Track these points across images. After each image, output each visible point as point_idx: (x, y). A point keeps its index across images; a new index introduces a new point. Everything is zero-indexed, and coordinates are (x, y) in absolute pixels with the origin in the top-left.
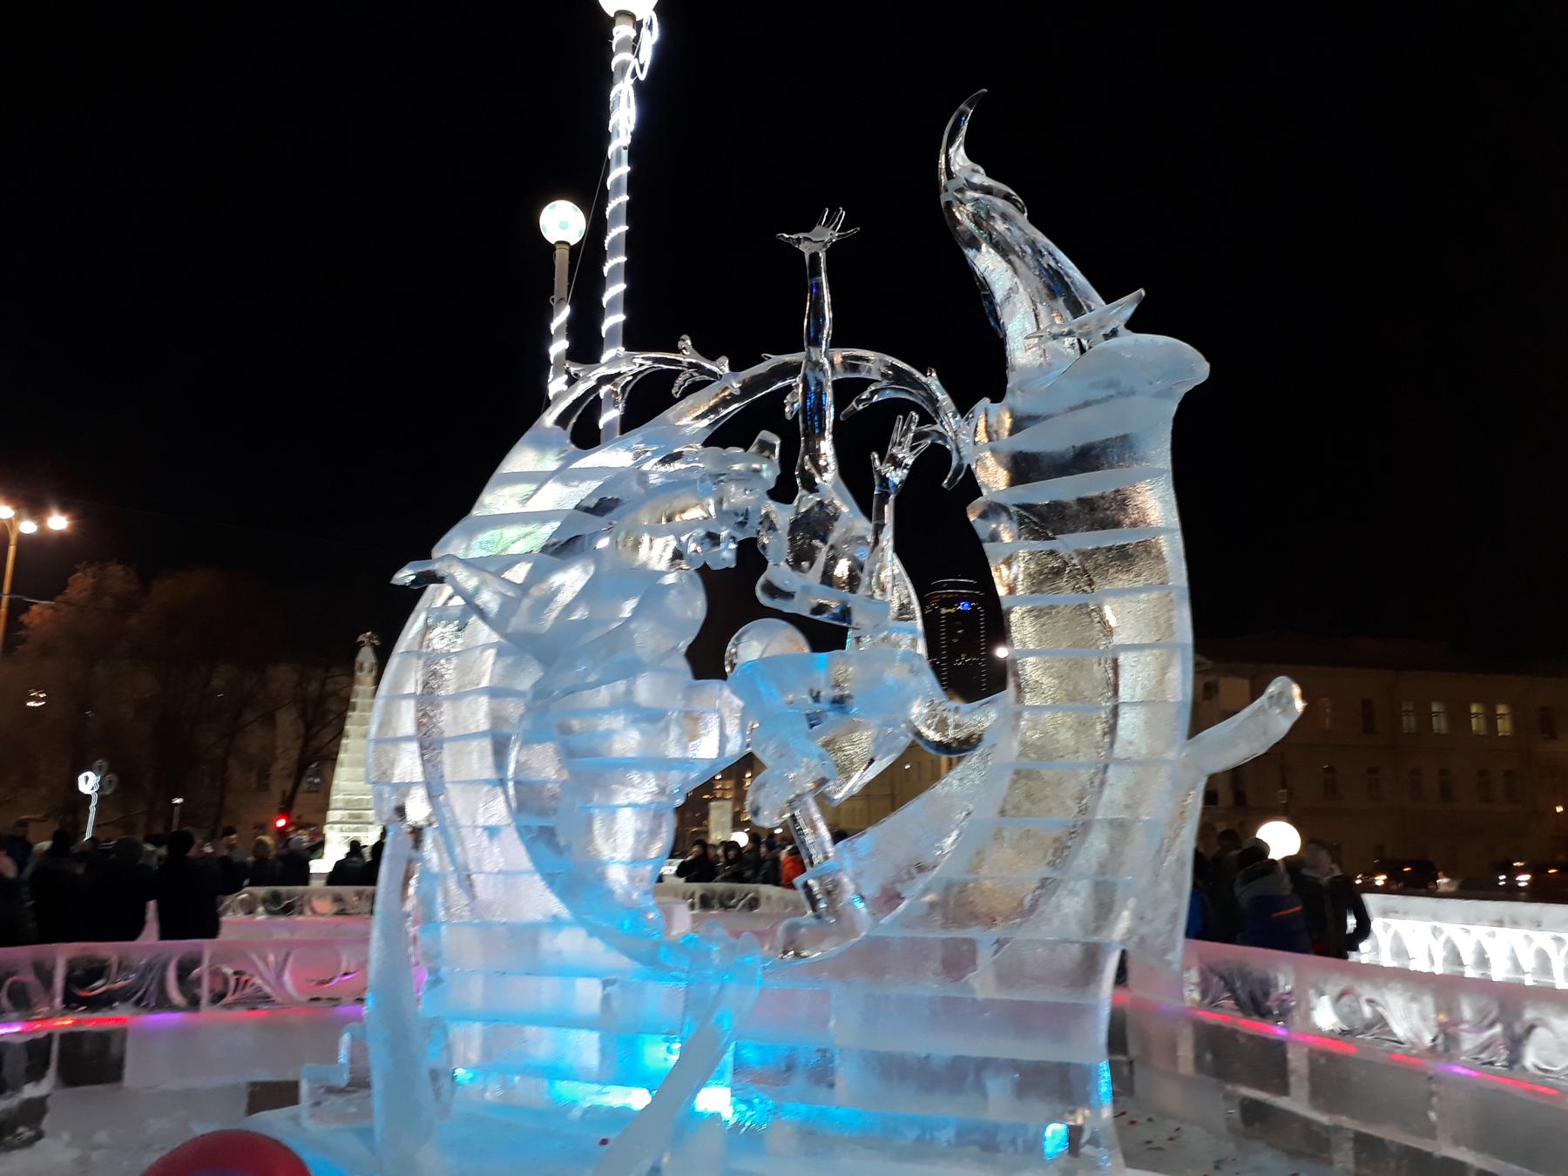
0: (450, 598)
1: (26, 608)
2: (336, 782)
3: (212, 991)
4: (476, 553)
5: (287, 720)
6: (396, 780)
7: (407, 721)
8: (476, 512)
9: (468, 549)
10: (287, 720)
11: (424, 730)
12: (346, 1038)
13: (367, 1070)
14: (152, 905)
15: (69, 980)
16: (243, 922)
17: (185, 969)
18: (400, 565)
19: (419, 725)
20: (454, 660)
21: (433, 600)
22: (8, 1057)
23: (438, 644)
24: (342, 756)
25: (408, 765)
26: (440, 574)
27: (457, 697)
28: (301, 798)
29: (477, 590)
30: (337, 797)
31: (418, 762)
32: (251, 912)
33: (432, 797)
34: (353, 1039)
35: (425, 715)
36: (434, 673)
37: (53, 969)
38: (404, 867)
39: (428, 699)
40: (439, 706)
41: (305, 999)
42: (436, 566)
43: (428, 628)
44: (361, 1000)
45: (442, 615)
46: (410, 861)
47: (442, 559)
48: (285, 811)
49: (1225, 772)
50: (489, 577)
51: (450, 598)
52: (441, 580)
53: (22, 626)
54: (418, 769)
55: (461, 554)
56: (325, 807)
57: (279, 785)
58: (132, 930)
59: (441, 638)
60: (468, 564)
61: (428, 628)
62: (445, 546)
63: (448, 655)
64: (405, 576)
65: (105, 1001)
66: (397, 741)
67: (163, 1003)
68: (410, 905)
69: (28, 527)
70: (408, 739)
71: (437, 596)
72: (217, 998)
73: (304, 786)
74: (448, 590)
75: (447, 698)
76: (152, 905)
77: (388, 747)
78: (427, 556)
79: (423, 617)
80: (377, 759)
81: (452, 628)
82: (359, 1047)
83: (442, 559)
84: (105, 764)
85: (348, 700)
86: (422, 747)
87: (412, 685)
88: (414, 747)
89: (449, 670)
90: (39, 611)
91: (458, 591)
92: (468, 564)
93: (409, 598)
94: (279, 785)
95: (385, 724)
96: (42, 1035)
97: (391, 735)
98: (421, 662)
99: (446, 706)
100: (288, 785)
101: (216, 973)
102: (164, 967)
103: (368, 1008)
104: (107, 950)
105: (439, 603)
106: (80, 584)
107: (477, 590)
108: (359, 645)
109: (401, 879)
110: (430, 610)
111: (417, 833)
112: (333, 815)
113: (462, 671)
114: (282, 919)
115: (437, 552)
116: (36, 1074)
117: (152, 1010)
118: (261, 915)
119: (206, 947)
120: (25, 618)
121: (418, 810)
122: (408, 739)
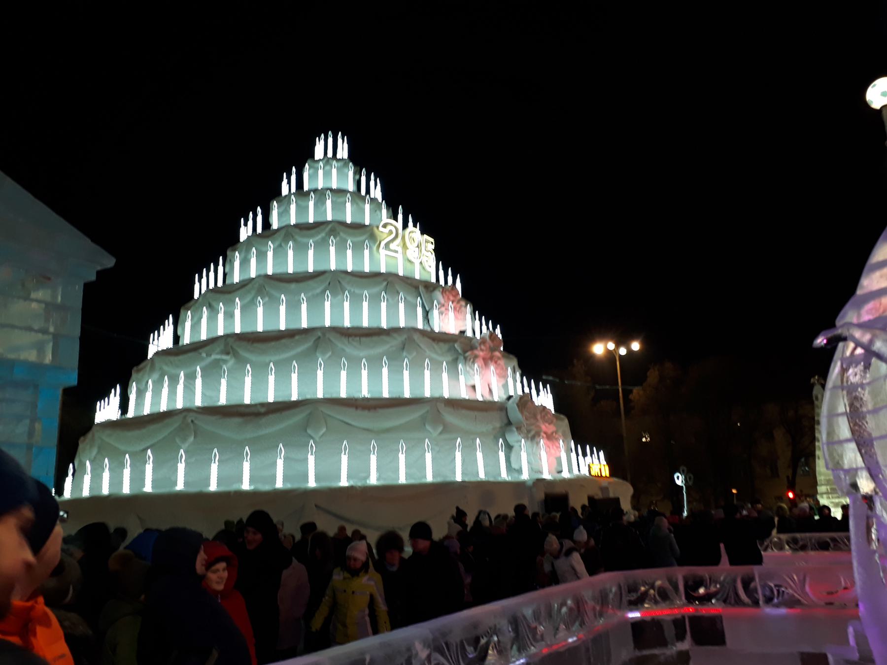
0: (855, 349)
1: (631, 391)
2: (817, 469)
3: (764, 596)
4: (866, 317)
5: (779, 435)
6: (846, 467)
7: (844, 430)
8: (859, 292)
9: (859, 316)
10: (779, 435)
11: (857, 434)
12: (851, 630)
13: (870, 651)
14: (722, 546)
15: (686, 586)
16: (778, 557)
17: (747, 582)
18: (816, 336)
19: (853, 432)
20: (867, 389)
21: (844, 352)
22: (665, 627)
23: (854, 379)
24: (818, 453)
25: (852, 456)
26: (844, 335)
27: (875, 411)
28: (798, 480)
29: (871, 342)
30: (820, 478)
31: (859, 454)
32: (781, 548)
33: (873, 477)
34: (855, 631)
35: (856, 424)
36: (856, 398)
37: (677, 580)
38: (865, 523)
39: (855, 416)
40: (864, 418)
41: (823, 603)
42: (839, 331)
43: (844, 371)
44: (857, 605)
45: (852, 361)
46: (868, 518)
47: (842, 326)
48: (792, 488)
49: (383, 632)
50: (878, 332)
51: (855, 349)
52: (845, 339)
53: (631, 401)
54: (859, 459)
55: (855, 320)
56: (814, 484)
57: (784, 472)
58: (716, 561)
59: (854, 375)
60: (862, 326)
61: (844, 371)
62: (843, 317)
63: (862, 386)
64: (821, 341)
65: (706, 598)
66: (841, 442)
67: (738, 602)
68: (874, 546)
69: (623, 351)
70: (848, 441)
71: (848, 349)
72: (769, 600)
73: (800, 471)
74: (852, 345)
75: (869, 412)
76: (722, 546)
77: (836, 447)
78: (833, 325)
79: (839, 364)
80: (831, 455)
81: (861, 367)
82: (861, 638)
83: (842, 326)
84: (685, 469)
85: (813, 418)
86: (858, 445)
87: (842, 406)
88: (853, 446)
89: (866, 395)
90: (637, 392)
91: (858, 344)
92: (862, 326)
93: (828, 354)
94: (784, 472)
95: (830, 433)
96: (679, 616)
97: (836, 439)
98: (845, 392)
99: (869, 418)
100: (790, 473)
101: (764, 586)
102: (735, 581)
103: (862, 608)
104: (703, 571)
105: (848, 353)
106: (653, 376)
107: (871, 342)
108: (813, 386)
109: (865, 530)
110: (843, 360)
111: (868, 499)
112: (821, 489)
113: (874, 395)
114: (801, 553)
115: (839, 322)
116: (681, 637)
117: (733, 605)
118: (787, 551)
119: (756, 570)
120: (631, 397)
121: (866, 485)
122: (848, 441)
